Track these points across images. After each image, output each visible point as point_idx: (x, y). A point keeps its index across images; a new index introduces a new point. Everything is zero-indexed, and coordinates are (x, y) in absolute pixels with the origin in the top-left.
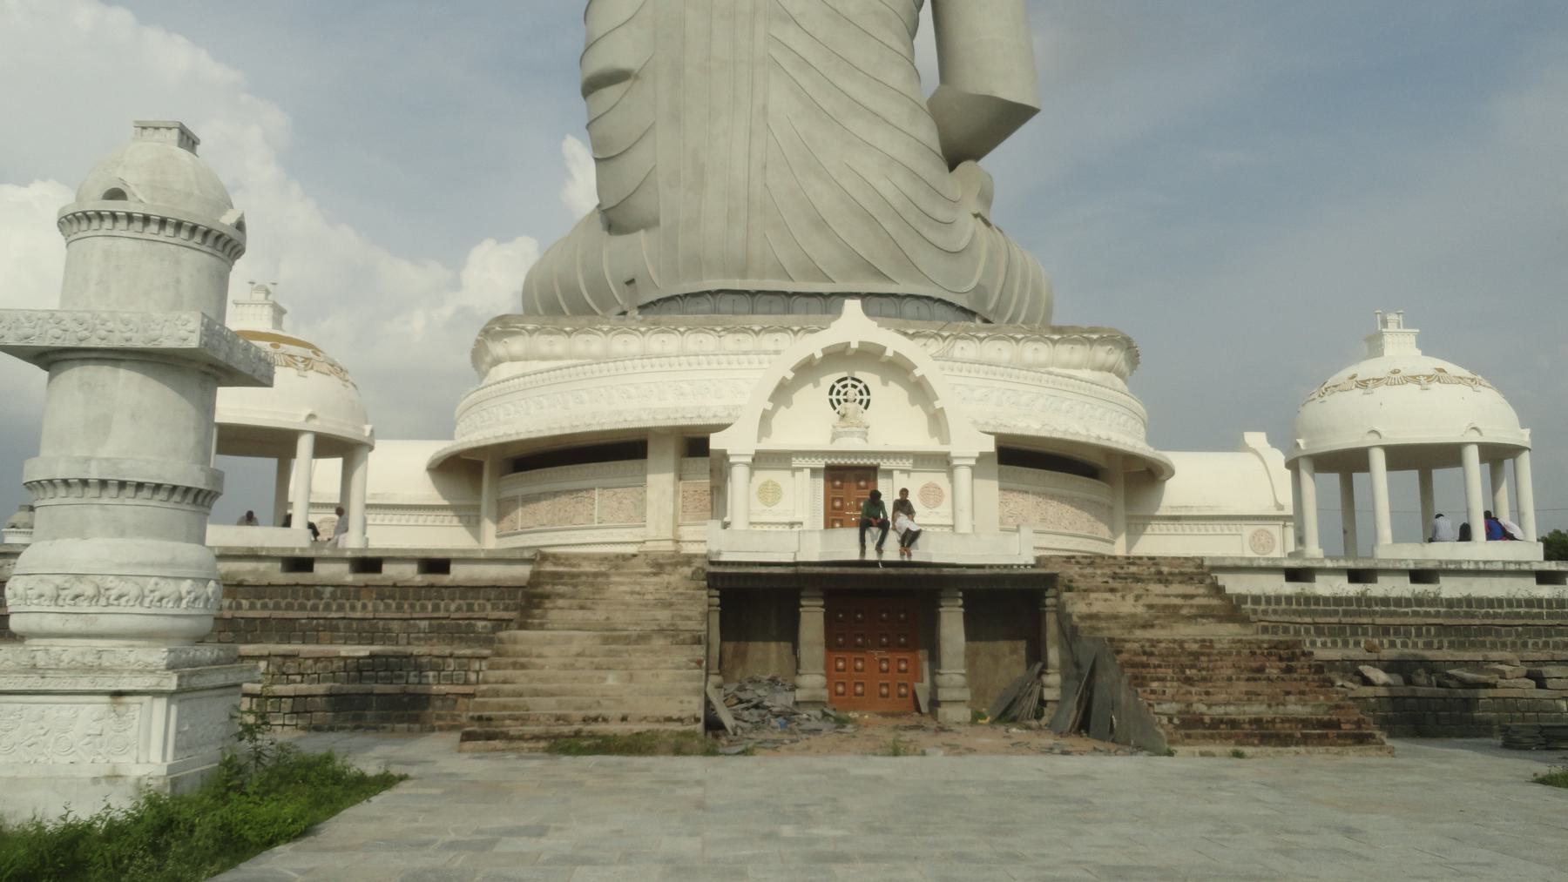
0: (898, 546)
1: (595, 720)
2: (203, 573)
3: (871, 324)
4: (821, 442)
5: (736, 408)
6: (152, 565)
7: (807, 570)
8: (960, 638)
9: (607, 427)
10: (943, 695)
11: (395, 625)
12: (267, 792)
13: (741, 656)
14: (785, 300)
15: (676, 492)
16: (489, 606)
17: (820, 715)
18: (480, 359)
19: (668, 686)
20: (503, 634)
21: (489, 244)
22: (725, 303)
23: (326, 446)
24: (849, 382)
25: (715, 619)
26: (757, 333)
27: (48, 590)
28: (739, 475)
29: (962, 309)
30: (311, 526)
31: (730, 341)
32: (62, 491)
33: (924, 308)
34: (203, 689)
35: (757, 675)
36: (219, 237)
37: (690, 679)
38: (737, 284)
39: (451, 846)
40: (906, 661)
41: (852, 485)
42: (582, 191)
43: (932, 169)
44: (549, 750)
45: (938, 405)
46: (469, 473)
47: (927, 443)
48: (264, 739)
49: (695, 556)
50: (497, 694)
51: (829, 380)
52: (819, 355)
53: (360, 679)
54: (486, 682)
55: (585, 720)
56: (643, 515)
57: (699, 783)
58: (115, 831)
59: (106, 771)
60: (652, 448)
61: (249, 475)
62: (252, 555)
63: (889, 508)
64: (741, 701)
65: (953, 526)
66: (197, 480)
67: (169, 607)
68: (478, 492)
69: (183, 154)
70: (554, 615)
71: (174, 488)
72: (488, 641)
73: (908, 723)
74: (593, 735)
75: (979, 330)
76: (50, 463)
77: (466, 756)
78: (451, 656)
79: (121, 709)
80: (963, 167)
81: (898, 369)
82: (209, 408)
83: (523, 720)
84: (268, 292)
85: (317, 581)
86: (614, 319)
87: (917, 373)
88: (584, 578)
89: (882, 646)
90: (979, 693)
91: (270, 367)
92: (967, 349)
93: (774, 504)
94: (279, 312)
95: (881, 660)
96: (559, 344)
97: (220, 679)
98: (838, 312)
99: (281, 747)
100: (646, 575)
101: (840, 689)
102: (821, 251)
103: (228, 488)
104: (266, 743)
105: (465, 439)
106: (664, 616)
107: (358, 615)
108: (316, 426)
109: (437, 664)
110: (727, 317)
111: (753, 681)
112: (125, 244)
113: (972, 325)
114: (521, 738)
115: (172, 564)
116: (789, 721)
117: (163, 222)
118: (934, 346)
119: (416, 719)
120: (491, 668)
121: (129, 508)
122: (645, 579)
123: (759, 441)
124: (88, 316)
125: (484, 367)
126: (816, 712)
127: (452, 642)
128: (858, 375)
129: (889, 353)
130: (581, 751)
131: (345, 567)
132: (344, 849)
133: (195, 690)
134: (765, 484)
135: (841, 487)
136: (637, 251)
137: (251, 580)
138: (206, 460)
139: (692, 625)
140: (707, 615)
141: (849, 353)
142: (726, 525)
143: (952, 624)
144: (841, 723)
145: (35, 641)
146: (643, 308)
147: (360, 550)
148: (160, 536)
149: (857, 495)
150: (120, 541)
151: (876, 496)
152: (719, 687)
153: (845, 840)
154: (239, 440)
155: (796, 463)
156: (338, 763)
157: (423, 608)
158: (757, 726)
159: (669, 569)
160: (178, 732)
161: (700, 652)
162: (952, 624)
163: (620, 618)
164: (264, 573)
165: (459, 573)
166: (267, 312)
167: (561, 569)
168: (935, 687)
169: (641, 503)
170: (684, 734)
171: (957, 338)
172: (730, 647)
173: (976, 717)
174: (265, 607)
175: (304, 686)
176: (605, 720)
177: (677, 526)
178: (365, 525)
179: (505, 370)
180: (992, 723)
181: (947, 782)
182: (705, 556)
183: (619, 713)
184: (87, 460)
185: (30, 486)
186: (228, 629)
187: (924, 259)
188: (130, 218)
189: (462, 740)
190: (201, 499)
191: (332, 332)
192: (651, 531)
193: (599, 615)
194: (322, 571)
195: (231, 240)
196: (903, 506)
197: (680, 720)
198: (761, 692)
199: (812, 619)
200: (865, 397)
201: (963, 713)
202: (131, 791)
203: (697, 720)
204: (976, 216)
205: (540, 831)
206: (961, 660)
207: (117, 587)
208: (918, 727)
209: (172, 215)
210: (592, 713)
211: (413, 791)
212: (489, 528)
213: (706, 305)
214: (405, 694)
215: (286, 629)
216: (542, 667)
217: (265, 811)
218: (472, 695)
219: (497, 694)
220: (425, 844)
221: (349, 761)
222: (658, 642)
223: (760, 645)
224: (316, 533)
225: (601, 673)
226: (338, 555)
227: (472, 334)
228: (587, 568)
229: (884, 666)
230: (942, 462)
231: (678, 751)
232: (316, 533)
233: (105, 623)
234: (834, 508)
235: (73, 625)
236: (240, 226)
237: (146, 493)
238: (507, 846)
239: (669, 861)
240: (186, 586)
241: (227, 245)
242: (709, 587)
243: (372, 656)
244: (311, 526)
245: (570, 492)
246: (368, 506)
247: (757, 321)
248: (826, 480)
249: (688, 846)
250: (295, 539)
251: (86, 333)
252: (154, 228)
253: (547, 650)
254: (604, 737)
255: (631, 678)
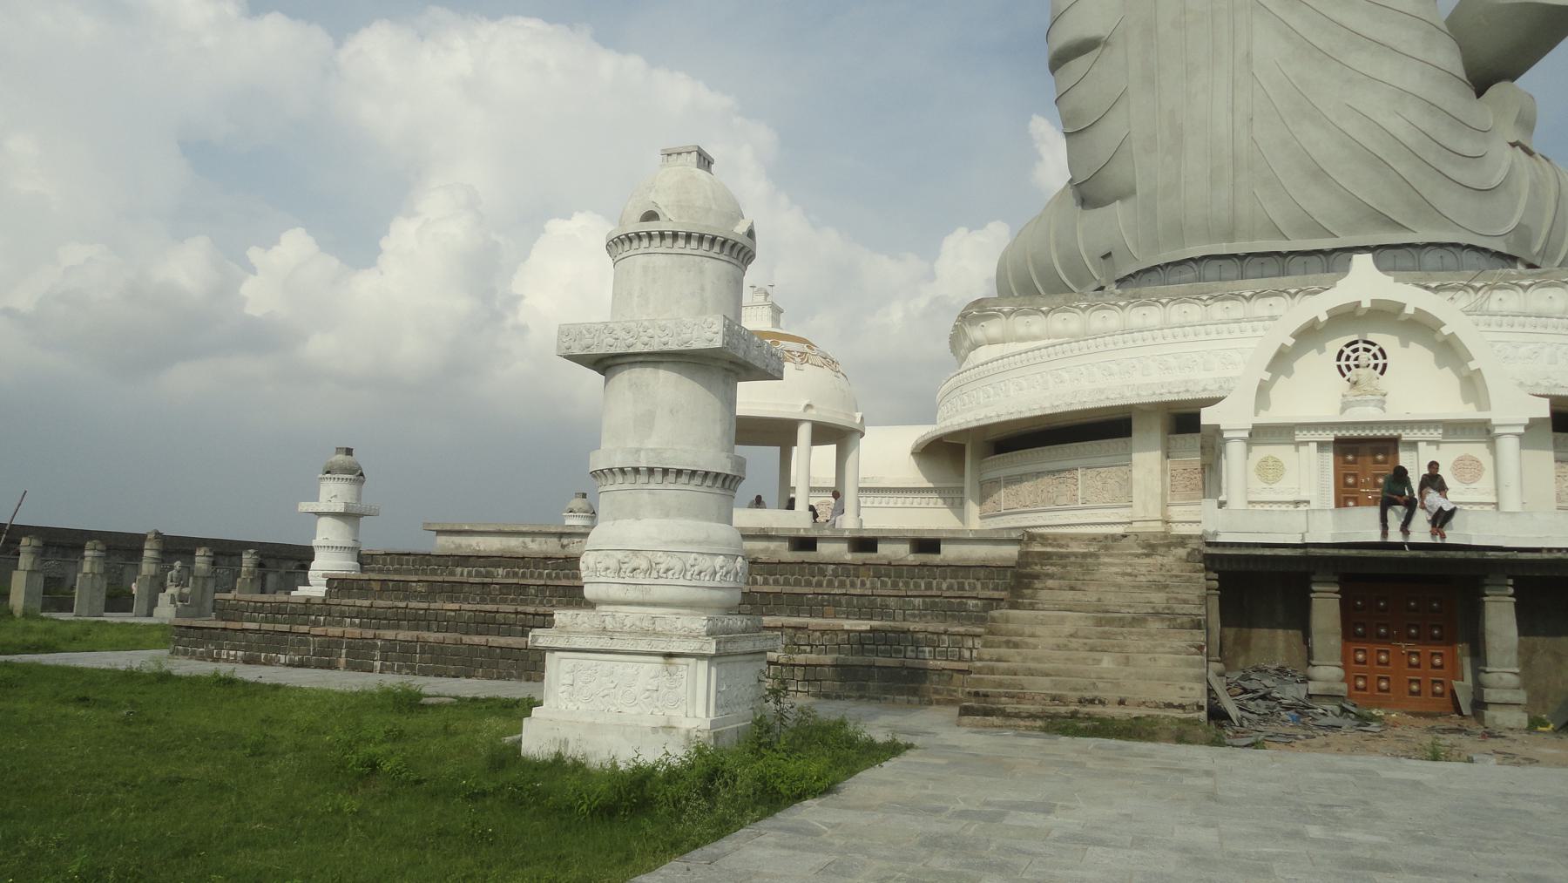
0: (1429, 527)
1: (1092, 702)
2: (731, 550)
3: (1388, 280)
4: (1330, 413)
5: (1227, 380)
6: (691, 542)
7: (1318, 552)
8: (1512, 631)
9: (1089, 406)
10: (1490, 695)
11: (892, 602)
12: (793, 751)
13: (1245, 644)
14: (1280, 260)
15: (1164, 471)
16: (979, 585)
17: (1337, 710)
18: (959, 343)
19: (1170, 671)
20: (995, 613)
21: (962, 231)
22: (1211, 269)
23: (824, 433)
24: (1361, 345)
25: (1214, 603)
26: (1248, 299)
27: (613, 563)
28: (1234, 454)
29: (1499, 255)
30: (812, 508)
31: (1218, 310)
32: (619, 478)
33: (1449, 258)
34: (736, 654)
35: (1262, 665)
36: (724, 243)
37: (1192, 665)
38: (1223, 248)
39: (963, 814)
40: (1441, 655)
41: (1367, 460)
42: (1053, 167)
43: (1457, 99)
44: (1045, 730)
45: (1472, 366)
46: (946, 454)
47: (1459, 409)
48: (786, 703)
49: (1190, 537)
50: (992, 671)
51: (1339, 343)
52: (1323, 317)
53: (862, 652)
54: (981, 660)
55: (1081, 701)
56: (1129, 494)
57: (1208, 773)
58: (673, 776)
59: (662, 723)
60: (1135, 425)
61: (762, 457)
62: (764, 535)
63: (1415, 486)
64: (1245, 691)
65: (1496, 505)
66: (727, 469)
67: (706, 581)
68: (962, 475)
69: (702, 173)
70: (1043, 595)
71: (694, 473)
72: (981, 620)
73: (1447, 725)
74: (1090, 717)
75: (1522, 276)
76: (609, 455)
77: (964, 730)
78: (945, 632)
79: (672, 669)
80: (1494, 91)
81: (1421, 328)
82: (731, 402)
83: (1019, 698)
84: (767, 294)
85: (820, 559)
86: (1091, 295)
87: (1445, 331)
88: (1072, 559)
89: (1410, 638)
90: (1537, 698)
91: (780, 361)
92: (1507, 300)
93: (1275, 481)
94: (777, 312)
95: (1410, 653)
96: (1036, 324)
97: (748, 646)
98: (1345, 270)
99: (802, 710)
100: (1138, 556)
101: (1361, 683)
102: (1319, 204)
103: (749, 473)
104: (787, 706)
105: (948, 423)
106: (1158, 598)
107: (858, 591)
108: (813, 415)
109: (933, 640)
110: (1214, 284)
111: (1258, 670)
112: (658, 259)
113: (1513, 272)
114: (1017, 715)
115: (707, 541)
116: (1302, 714)
117: (688, 237)
118: (1464, 300)
119: (915, 692)
120: (985, 646)
121: (672, 492)
122: (1137, 560)
123: (1256, 414)
124: (633, 325)
125: (962, 352)
126: (1333, 707)
127: (945, 619)
128: (1370, 337)
129: (1409, 310)
130: (1078, 733)
131: (844, 546)
132: (865, 808)
133: (729, 655)
134: (1265, 461)
135: (1354, 462)
136: (1114, 224)
137: (763, 557)
138: (731, 450)
139: (1188, 608)
140: (1205, 599)
141: (1359, 313)
142: (1221, 505)
143: (1500, 616)
144: (1364, 720)
145: (604, 608)
146: (1121, 282)
147: (858, 530)
148: (696, 517)
149: (1374, 471)
150: (665, 521)
151: (1401, 475)
152: (1220, 675)
153: (1383, 847)
154: (755, 431)
155: (1300, 436)
156: (851, 729)
157: (917, 586)
158: (1265, 718)
159: (1161, 550)
160: (718, 692)
161: (1199, 637)
162: (1500, 616)
163: (1112, 599)
164: (774, 552)
165: (949, 553)
166: (767, 311)
167: (1049, 549)
168: (1479, 686)
169: (1127, 482)
170: (1186, 721)
171: (1493, 288)
172: (1231, 632)
173: (1534, 724)
174: (776, 582)
175: (813, 656)
176: (1102, 702)
177: (1166, 506)
178: (859, 507)
179: (983, 354)
180: (1555, 731)
181: (1505, 795)
182: (1201, 537)
183: (1114, 695)
184: (638, 451)
185: (595, 474)
186: (752, 602)
187: (1447, 201)
188: (662, 235)
189: (961, 714)
190: (727, 482)
191: (820, 328)
192: (1138, 511)
193: (1090, 596)
194: (825, 550)
195: (736, 244)
196: (1433, 480)
197: (1181, 707)
198: (1268, 682)
199: (1326, 608)
200: (1381, 361)
201: (1518, 718)
202: (682, 741)
203: (1201, 708)
204: (1513, 145)
205: (1047, 809)
206: (1513, 657)
207: (665, 562)
208: (1459, 730)
209: (696, 229)
210: (1088, 695)
211: (920, 760)
212: (973, 509)
213: (1189, 273)
214: (903, 667)
215: (796, 604)
216: (1035, 647)
217: (792, 767)
218: (968, 672)
219: (992, 671)
220: (937, 811)
221: (860, 727)
222: (1154, 625)
223: (1265, 632)
224: (815, 516)
225: (1097, 655)
226: (838, 535)
227: (948, 323)
228: (1076, 548)
229: (1414, 660)
230: (1483, 431)
231: (1181, 737)
232: (815, 516)
233: (657, 593)
234: (1346, 485)
235: (633, 594)
236: (751, 234)
237: (684, 479)
238: (1015, 819)
239: (1185, 850)
240: (720, 560)
241: (740, 252)
242: (1207, 569)
243: (873, 630)
244: (812, 508)
245: (1052, 472)
246: (861, 490)
247: (1248, 286)
248: (1336, 454)
249: (1205, 837)
250: (798, 521)
251: (632, 340)
252: (681, 242)
253: (1039, 630)
254: (1102, 720)
255: (1127, 662)
